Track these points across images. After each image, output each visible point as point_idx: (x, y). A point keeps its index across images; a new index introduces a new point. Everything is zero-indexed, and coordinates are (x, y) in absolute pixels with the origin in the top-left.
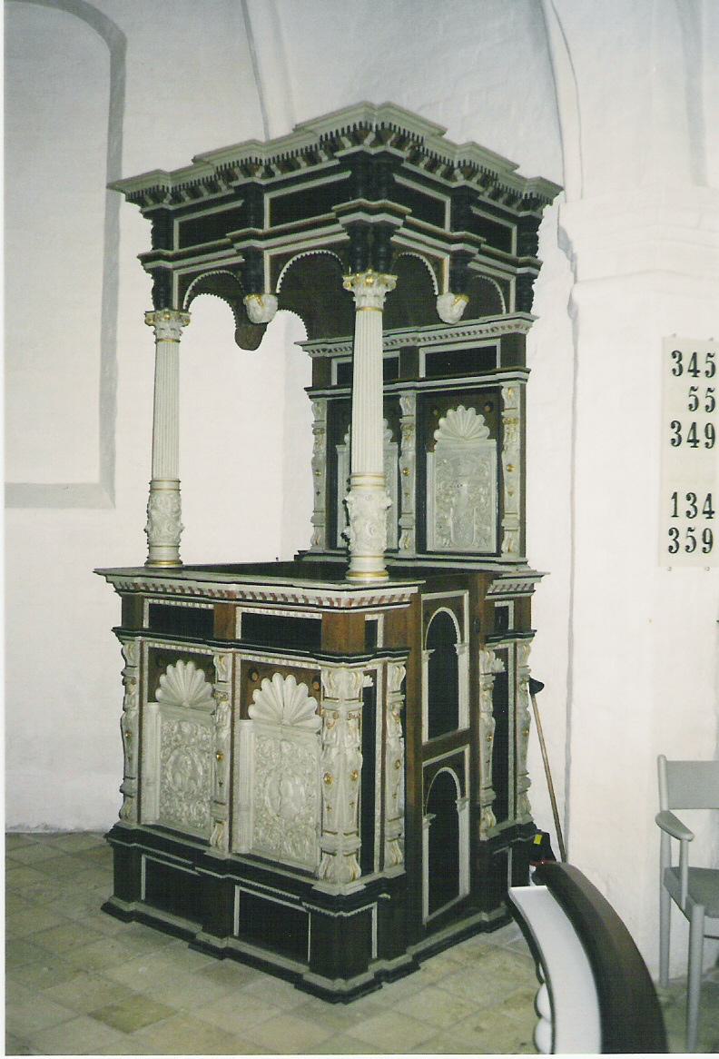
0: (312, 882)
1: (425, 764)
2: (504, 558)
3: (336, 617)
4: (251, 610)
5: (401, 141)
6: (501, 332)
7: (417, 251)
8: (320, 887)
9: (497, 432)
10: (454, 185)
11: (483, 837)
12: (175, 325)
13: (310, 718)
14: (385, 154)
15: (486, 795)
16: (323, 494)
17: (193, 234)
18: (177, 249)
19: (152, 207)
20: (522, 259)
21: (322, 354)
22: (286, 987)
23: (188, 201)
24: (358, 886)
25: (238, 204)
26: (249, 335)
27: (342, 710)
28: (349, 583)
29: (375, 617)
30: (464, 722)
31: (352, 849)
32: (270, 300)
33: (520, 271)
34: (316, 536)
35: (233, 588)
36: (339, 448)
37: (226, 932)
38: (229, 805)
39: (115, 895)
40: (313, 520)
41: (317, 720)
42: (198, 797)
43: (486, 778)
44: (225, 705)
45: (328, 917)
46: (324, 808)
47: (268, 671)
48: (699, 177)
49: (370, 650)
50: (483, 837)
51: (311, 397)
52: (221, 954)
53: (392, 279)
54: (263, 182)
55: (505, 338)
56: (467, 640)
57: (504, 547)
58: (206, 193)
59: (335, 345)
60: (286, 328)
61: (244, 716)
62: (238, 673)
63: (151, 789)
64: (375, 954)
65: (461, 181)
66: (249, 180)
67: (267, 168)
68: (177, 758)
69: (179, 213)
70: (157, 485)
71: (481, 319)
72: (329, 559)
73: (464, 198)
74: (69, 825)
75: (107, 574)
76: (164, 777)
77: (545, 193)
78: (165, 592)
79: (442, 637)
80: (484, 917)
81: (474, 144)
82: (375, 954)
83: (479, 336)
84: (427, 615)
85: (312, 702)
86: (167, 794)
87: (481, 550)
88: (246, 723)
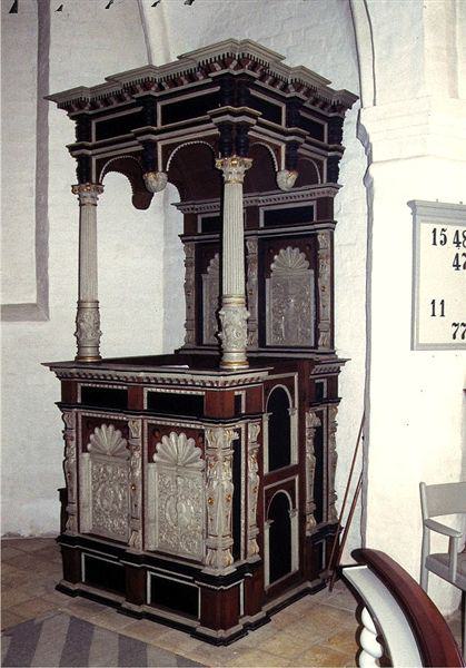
0: (201, 567)
1: (265, 488)
2: (320, 349)
3: (217, 395)
4: (154, 390)
5: (254, 67)
6: (317, 196)
7: (264, 141)
8: (207, 571)
9: (314, 263)
10: (288, 96)
11: (308, 534)
12: (94, 194)
13: (197, 461)
14: (244, 75)
15: (310, 507)
16: (193, 307)
17: (104, 131)
18: (94, 142)
19: (77, 112)
20: (331, 146)
21: (191, 211)
22: (186, 636)
23: (102, 108)
24: (232, 569)
25: (140, 109)
26: (142, 199)
27: (220, 455)
28: (226, 370)
29: (240, 393)
30: (295, 459)
31: (228, 546)
32: (162, 176)
33: (329, 154)
34: (188, 336)
35: (142, 374)
36: (204, 276)
37: (142, 602)
38: (141, 519)
39: (65, 578)
40: (186, 325)
41: (201, 463)
42: (119, 515)
43: (309, 497)
44: (137, 454)
45: (213, 590)
46: (208, 519)
47: (167, 430)
48: (454, 94)
49: (238, 415)
50: (308, 534)
51: (183, 241)
52: (138, 616)
53: (248, 161)
54: (157, 95)
55: (319, 200)
56: (296, 406)
57: (320, 342)
58: (115, 102)
59: (205, 207)
60: (166, 195)
61: (151, 460)
62: (146, 432)
63: (152, 525)
64: (242, 613)
65: (292, 93)
66: (146, 93)
67: (160, 85)
68: (104, 490)
69: (162, 98)
70: (84, 305)
71: (303, 188)
72: (197, 352)
73: (294, 104)
74: (26, 533)
75: (52, 366)
76: (95, 502)
77: (348, 100)
78: (92, 378)
79: (278, 407)
80: (309, 585)
81: (302, 68)
82: (242, 613)
83: (301, 199)
84: (267, 390)
85: (198, 451)
86: (97, 513)
87: (304, 345)
88: (152, 465)
